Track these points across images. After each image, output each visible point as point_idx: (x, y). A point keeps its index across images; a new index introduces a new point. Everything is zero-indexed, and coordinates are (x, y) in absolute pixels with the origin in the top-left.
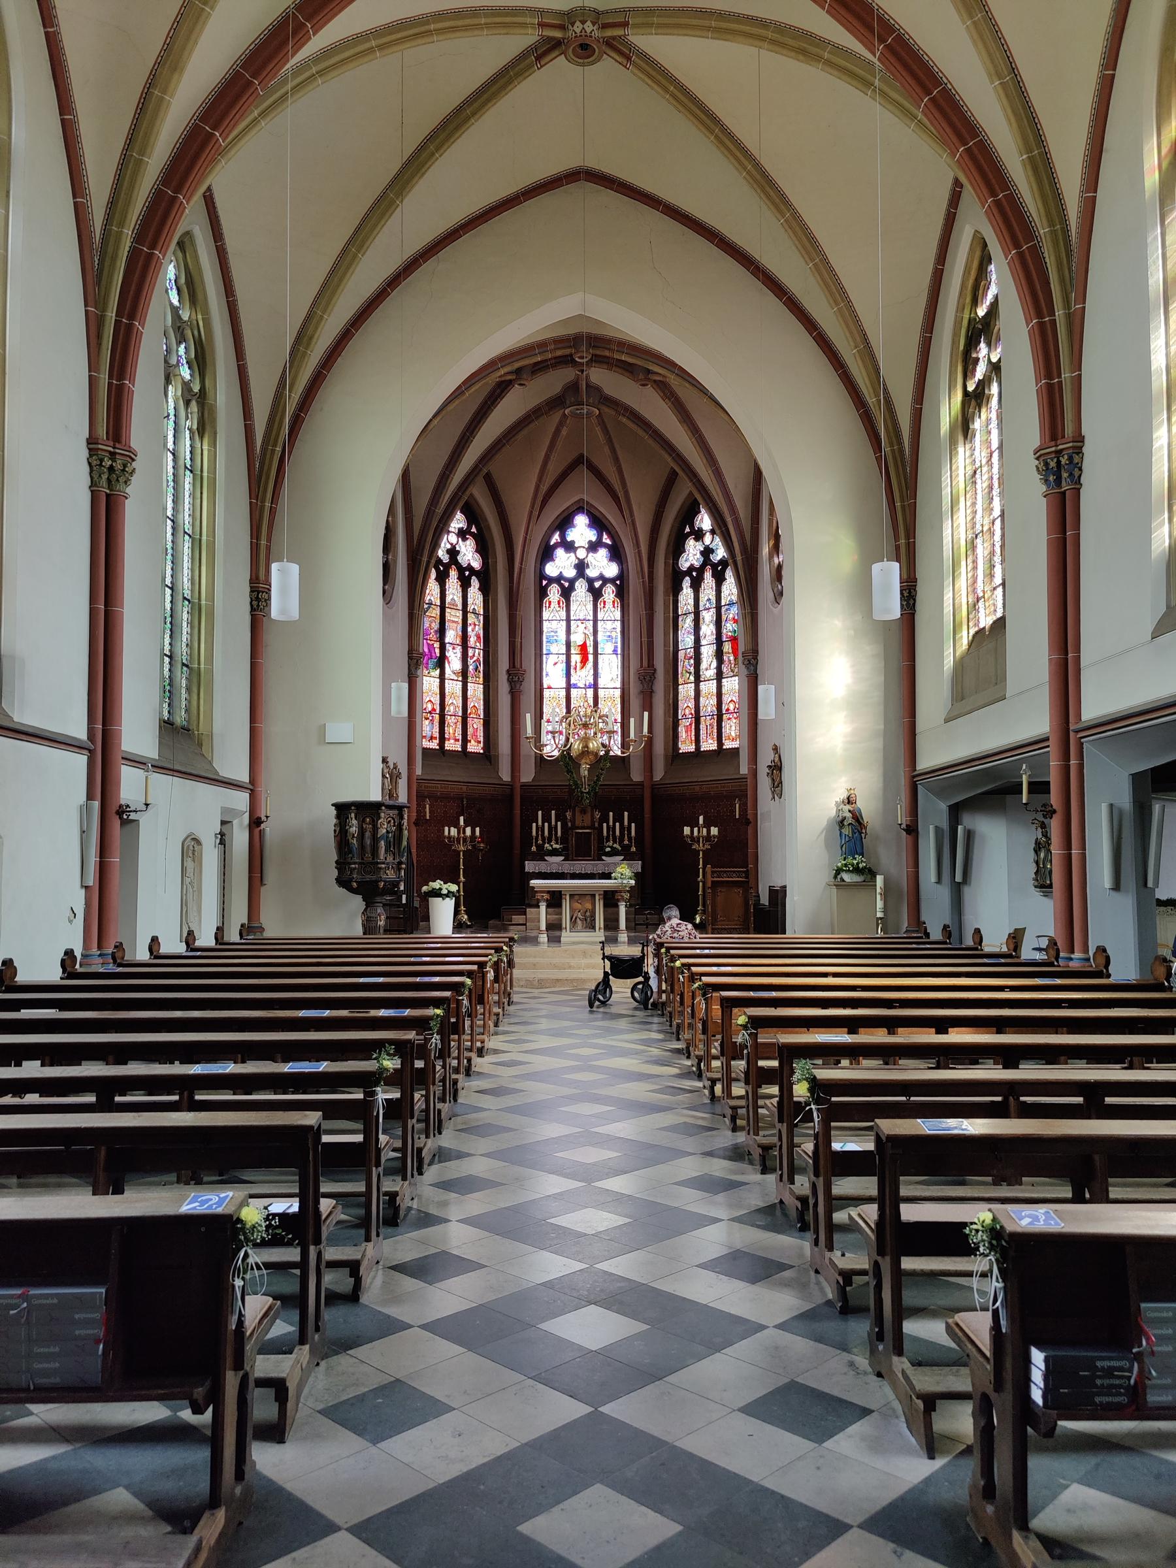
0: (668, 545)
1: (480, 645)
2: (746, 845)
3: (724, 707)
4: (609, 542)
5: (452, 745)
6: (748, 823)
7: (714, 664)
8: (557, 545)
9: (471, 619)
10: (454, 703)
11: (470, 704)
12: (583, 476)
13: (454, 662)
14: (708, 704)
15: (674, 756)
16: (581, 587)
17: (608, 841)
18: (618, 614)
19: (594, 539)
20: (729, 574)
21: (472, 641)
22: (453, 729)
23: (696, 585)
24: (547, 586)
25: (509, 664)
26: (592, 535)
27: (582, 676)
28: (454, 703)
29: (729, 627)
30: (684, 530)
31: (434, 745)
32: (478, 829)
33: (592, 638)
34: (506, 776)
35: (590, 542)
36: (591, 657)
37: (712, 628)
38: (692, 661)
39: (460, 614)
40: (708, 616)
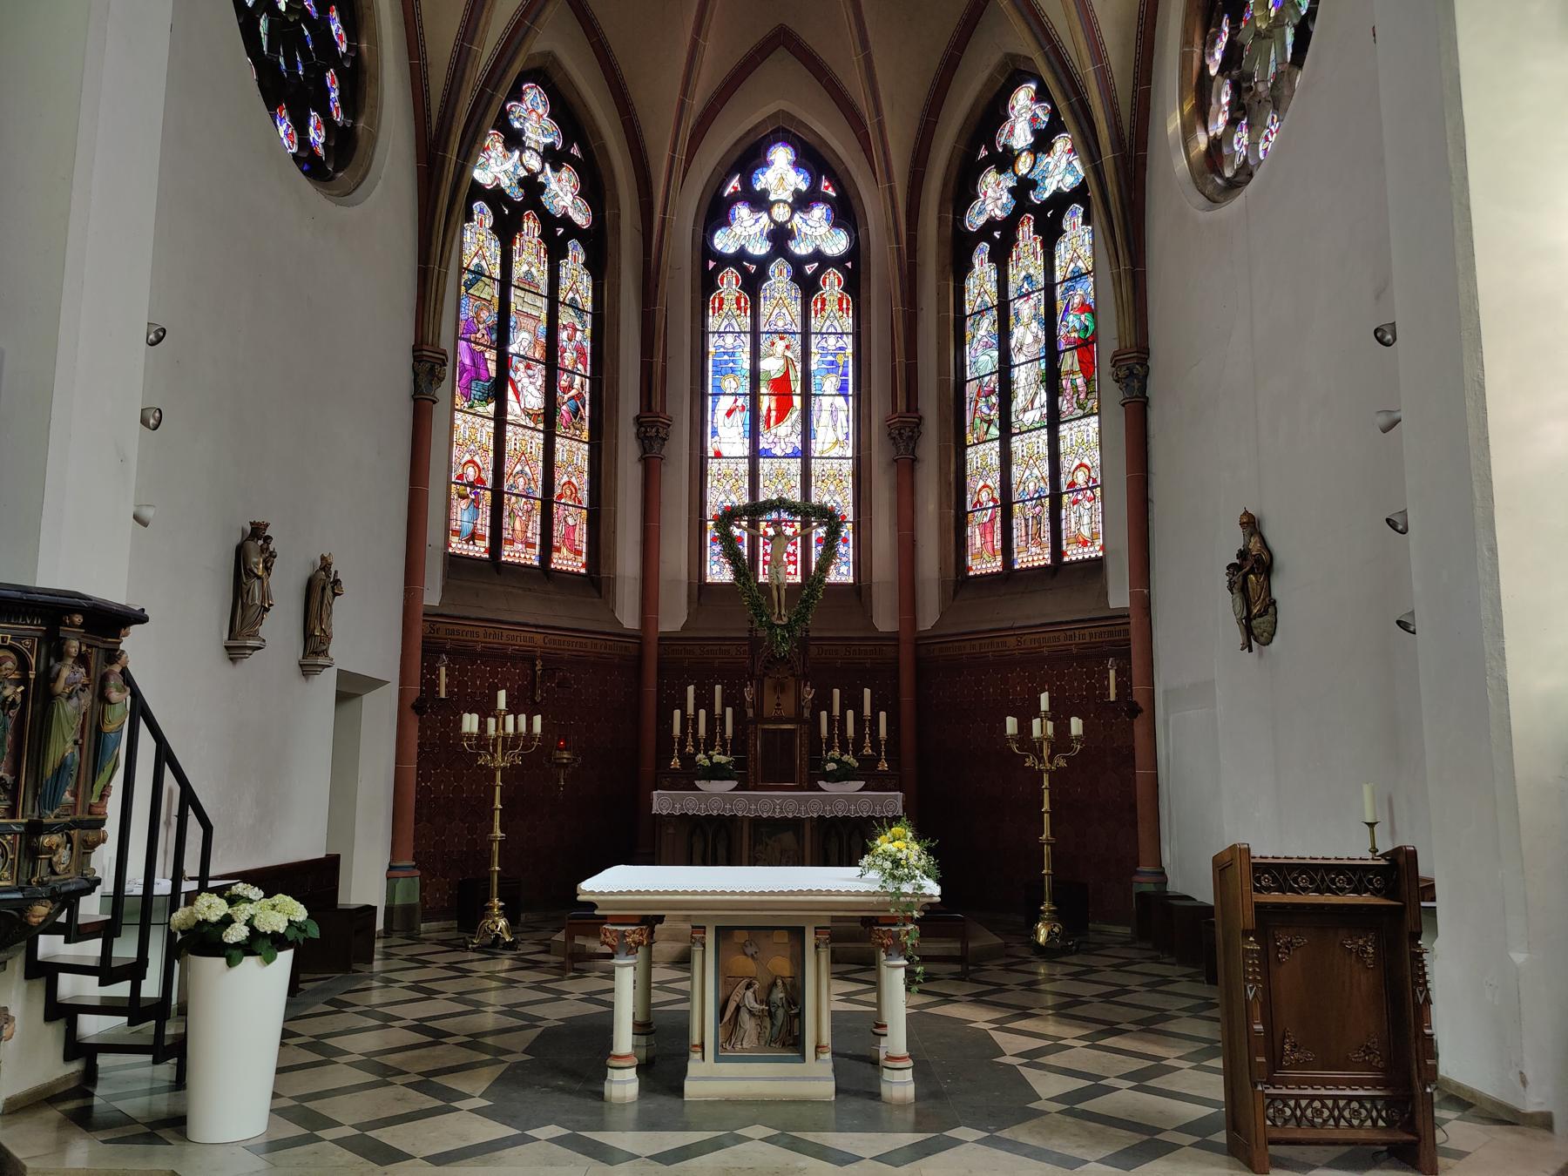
0: (945, 185)
1: (585, 369)
2: (1128, 758)
3: (1065, 480)
4: (831, 192)
5: (516, 553)
6: (1134, 710)
7: (1043, 396)
8: (735, 199)
9: (566, 317)
10: (524, 473)
11: (561, 478)
12: (781, 70)
13: (528, 392)
14: (1031, 476)
15: (960, 582)
16: (779, 274)
17: (830, 748)
18: (848, 323)
19: (804, 187)
20: (1073, 221)
21: (568, 358)
22: (522, 524)
23: (1001, 257)
24: (717, 270)
25: (641, 401)
26: (799, 181)
27: (782, 436)
28: (524, 473)
29: (1072, 324)
30: (981, 146)
31: (479, 549)
32: (538, 720)
33: (799, 367)
34: (628, 617)
35: (797, 192)
36: (797, 401)
37: (1036, 329)
38: (994, 399)
39: (543, 303)
40: (1027, 310)
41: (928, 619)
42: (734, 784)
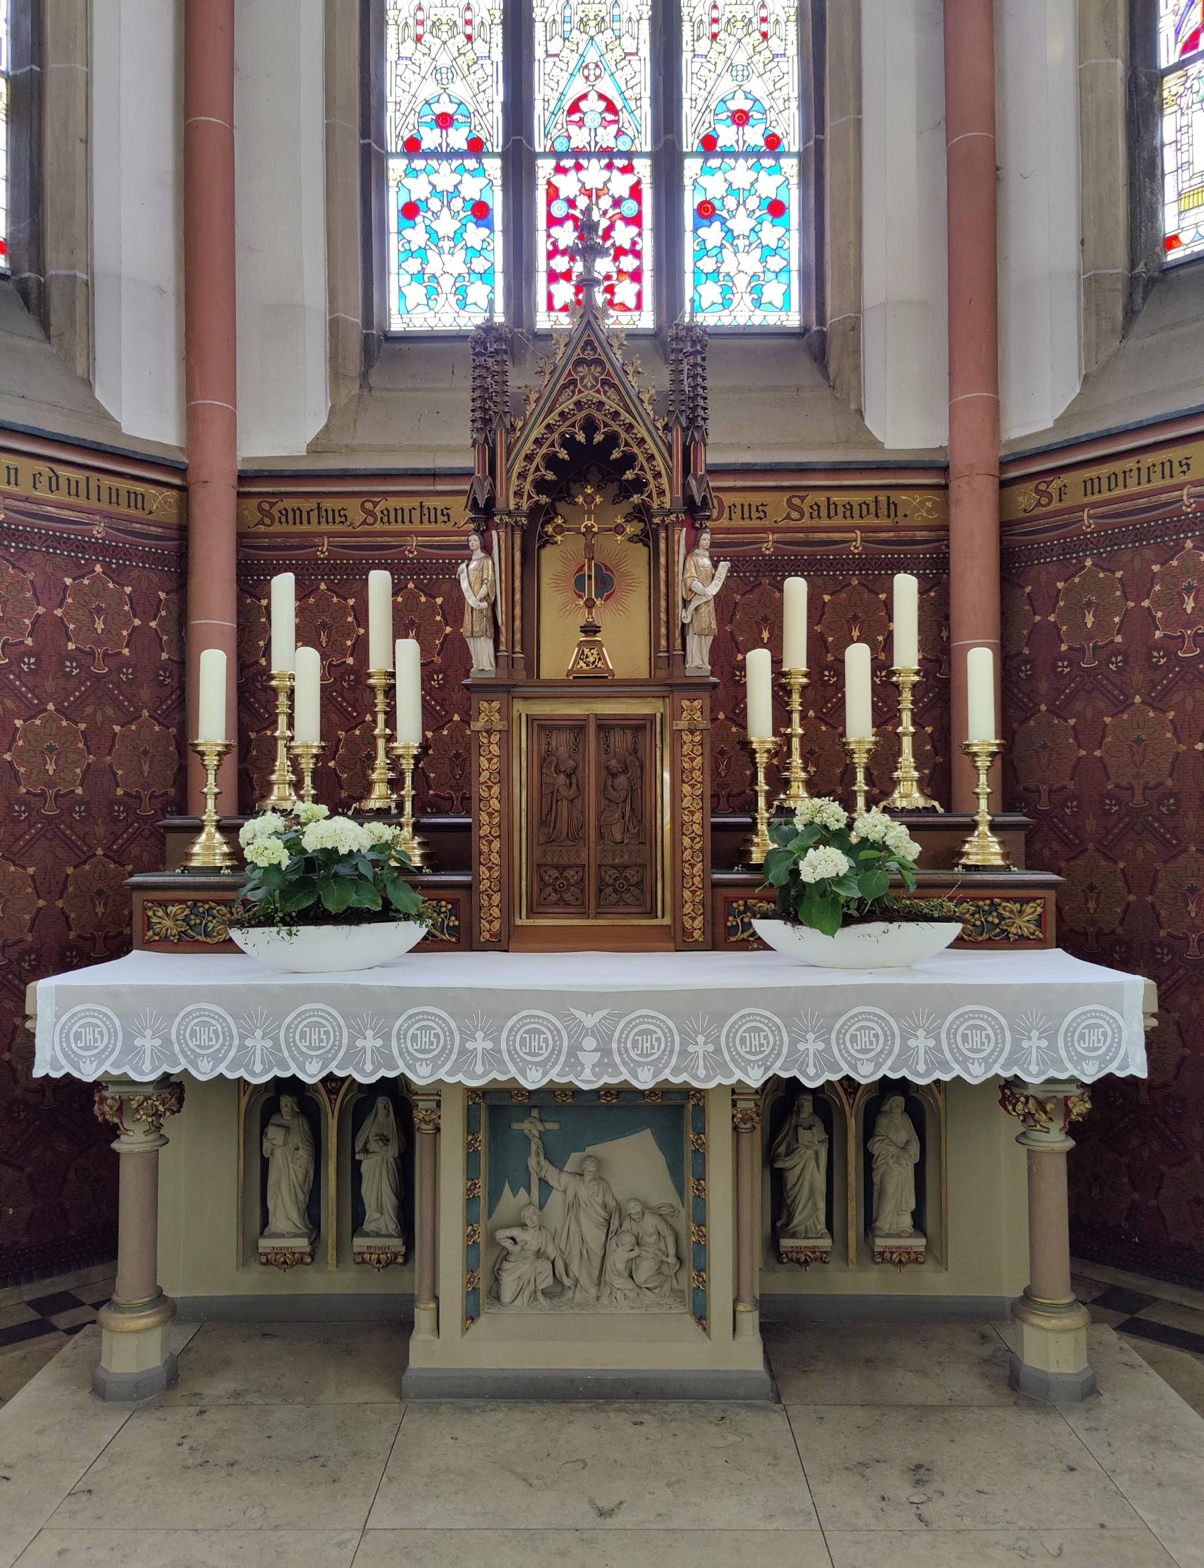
34: (141, 405)
41: (1040, 402)
42: (414, 932)
